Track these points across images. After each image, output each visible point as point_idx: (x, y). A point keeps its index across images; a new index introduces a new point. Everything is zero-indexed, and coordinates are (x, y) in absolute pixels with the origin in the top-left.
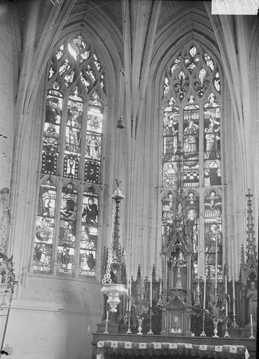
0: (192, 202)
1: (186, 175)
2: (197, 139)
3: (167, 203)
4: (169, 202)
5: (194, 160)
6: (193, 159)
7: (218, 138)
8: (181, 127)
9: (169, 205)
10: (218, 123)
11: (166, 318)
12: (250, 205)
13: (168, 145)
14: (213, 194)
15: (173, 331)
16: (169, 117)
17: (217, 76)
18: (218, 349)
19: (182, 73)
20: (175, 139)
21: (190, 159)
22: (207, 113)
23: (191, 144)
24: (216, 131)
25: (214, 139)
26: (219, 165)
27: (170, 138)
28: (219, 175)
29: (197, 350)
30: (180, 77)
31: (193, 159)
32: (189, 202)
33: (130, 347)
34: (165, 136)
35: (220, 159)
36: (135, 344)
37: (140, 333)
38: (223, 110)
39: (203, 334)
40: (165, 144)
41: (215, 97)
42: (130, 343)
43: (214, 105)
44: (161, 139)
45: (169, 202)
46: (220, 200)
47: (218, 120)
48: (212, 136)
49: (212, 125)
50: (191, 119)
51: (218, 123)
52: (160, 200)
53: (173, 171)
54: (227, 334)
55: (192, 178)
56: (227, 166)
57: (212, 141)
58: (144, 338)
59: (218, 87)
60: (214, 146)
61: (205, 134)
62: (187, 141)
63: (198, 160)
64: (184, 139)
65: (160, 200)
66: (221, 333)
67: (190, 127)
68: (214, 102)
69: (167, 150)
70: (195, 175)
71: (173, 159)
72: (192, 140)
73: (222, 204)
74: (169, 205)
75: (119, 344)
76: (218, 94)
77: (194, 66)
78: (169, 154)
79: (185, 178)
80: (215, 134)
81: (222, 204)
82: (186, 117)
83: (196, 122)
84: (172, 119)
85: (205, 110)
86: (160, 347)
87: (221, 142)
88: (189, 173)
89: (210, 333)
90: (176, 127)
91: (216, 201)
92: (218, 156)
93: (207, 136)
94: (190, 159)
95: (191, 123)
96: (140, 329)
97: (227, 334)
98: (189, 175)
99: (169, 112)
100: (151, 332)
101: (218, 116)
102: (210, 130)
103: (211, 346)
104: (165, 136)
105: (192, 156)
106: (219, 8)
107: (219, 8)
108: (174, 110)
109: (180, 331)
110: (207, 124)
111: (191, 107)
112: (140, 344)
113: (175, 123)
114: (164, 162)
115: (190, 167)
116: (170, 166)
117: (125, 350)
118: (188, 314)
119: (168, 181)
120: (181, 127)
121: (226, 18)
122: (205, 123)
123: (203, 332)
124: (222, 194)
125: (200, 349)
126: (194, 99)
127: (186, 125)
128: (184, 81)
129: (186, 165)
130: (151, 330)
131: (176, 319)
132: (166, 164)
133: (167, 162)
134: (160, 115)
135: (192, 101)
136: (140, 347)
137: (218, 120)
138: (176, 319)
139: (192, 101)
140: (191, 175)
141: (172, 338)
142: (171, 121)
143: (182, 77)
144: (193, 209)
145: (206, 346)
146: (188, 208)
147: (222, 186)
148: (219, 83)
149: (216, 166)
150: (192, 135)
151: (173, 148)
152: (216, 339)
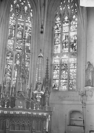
0: (18, 57)
1: (17, 46)
2: (22, 33)
3: (9, 56)
4: (9, 55)
5: (21, 41)
6: (20, 40)
7: (30, 35)
8: (17, 27)
9: (9, 57)
10: (31, 29)
11: (17, 102)
12: (47, 63)
13: (11, 33)
14: (10, 53)
15: (19, 107)
16: (12, 21)
17: (32, 11)
18: (35, 114)
19: (18, 5)
20: (14, 31)
21: (19, 40)
22: (27, 24)
23: (20, 34)
24: (30, 32)
25: (29, 35)
26: (30, 45)
27: (11, 30)
28: (30, 49)
29: (32, 114)
30: (17, 6)
31: (20, 40)
32: (18, 57)
33: (6, 113)
34: (10, 29)
35: (30, 43)
36: (9, 112)
37: (34, 109)
38: (33, 25)
39: (30, 108)
40: (9, 32)
41: (30, 19)
42: (6, 112)
43: (30, 22)
44: (8, 29)
45: (9, 55)
46: (29, 59)
47: (31, 28)
48: (28, 34)
49: (28, 29)
50: (21, 25)
51: (31, 29)
52: (6, 54)
53: (12, 44)
54: (38, 109)
55: (19, 48)
56: (5, 40)
57: (28, 36)
58: (36, 111)
59: (32, 15)
60: (28, 38)
61: (26, 32)
62: (18, 33)
63: (22, 42)
64: (17, 32)
65: (6, 54)
66: (8, 106)
67: (20, 28)
68: (30, 20)
69: (10, 34)
70: (20, 47)
71: (12, 39)
72: (21, 33)
73: (30, 60)
74: (9, 57)
75: (42, 114)
76: (32, 18)
77: (23, 4)
78: (11, 36)
79: (16, 47)
80: (29, 33)
81: (30, 60)
82: (19, 23)
83: (23, 26)
84: (13, 22)
85: (26, 22)
86: (19, 113)
87: (32, 37)
88: (18, 46)
89: (32, 108)
90: (15, 26)
91: (27, 59)
92: (30, 42)
93: (26, 33)
94: (19, 40)
95: (20, 26)
96: (6, 105)
97: (38, 109)
98: (18, 46)
99: (12, 19)
100: (10, 107)
101: (31, 26)
102: (28, 31)
103: (38, 113)
104: (10, 29)
105: (20, 39)
106: (82, 4)
107: (82, 4)
108: (14, 19)
109: (22, 107)
110: (26, 28)
111: (21, 20)
112: (11, 112)
113: (14, 24)
114: (8, 39)
115: (19, 43)
116: (11, 41)
117: (4, 114)
118: (26, 101)
119: (9, 47)
120: (17, 27)
121: (86, 8)
122: (18, 26)
123: (30, 108)
124: (30, 56)
125: (34, 114)
126: (22, 17)
127: (18, 26)
128: (19, 9)
129: (17, 42)
130: (10, 106)
131: (21, 103)
132: (9, 40)
133: (9, 39)
134: (8, 20)
135: (21, 18)
136: (11, 113)
137: (31, 28)
138: (21, 103)
139: (21, 18)
140: (19, 47)
141: (19, 110)
142: (13, 23)
143: (18, 6)
144: (18, 60)
145: (36, 113)
146: (17, 59)
147: (31, 54)
148: (32, 14)
149: (28, 45)
150: (21, 31)
151: (12, 34)
152: (6, 108)
